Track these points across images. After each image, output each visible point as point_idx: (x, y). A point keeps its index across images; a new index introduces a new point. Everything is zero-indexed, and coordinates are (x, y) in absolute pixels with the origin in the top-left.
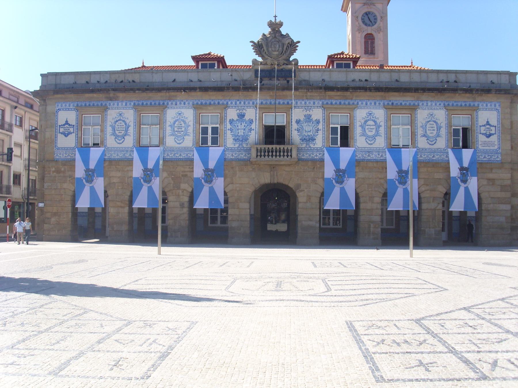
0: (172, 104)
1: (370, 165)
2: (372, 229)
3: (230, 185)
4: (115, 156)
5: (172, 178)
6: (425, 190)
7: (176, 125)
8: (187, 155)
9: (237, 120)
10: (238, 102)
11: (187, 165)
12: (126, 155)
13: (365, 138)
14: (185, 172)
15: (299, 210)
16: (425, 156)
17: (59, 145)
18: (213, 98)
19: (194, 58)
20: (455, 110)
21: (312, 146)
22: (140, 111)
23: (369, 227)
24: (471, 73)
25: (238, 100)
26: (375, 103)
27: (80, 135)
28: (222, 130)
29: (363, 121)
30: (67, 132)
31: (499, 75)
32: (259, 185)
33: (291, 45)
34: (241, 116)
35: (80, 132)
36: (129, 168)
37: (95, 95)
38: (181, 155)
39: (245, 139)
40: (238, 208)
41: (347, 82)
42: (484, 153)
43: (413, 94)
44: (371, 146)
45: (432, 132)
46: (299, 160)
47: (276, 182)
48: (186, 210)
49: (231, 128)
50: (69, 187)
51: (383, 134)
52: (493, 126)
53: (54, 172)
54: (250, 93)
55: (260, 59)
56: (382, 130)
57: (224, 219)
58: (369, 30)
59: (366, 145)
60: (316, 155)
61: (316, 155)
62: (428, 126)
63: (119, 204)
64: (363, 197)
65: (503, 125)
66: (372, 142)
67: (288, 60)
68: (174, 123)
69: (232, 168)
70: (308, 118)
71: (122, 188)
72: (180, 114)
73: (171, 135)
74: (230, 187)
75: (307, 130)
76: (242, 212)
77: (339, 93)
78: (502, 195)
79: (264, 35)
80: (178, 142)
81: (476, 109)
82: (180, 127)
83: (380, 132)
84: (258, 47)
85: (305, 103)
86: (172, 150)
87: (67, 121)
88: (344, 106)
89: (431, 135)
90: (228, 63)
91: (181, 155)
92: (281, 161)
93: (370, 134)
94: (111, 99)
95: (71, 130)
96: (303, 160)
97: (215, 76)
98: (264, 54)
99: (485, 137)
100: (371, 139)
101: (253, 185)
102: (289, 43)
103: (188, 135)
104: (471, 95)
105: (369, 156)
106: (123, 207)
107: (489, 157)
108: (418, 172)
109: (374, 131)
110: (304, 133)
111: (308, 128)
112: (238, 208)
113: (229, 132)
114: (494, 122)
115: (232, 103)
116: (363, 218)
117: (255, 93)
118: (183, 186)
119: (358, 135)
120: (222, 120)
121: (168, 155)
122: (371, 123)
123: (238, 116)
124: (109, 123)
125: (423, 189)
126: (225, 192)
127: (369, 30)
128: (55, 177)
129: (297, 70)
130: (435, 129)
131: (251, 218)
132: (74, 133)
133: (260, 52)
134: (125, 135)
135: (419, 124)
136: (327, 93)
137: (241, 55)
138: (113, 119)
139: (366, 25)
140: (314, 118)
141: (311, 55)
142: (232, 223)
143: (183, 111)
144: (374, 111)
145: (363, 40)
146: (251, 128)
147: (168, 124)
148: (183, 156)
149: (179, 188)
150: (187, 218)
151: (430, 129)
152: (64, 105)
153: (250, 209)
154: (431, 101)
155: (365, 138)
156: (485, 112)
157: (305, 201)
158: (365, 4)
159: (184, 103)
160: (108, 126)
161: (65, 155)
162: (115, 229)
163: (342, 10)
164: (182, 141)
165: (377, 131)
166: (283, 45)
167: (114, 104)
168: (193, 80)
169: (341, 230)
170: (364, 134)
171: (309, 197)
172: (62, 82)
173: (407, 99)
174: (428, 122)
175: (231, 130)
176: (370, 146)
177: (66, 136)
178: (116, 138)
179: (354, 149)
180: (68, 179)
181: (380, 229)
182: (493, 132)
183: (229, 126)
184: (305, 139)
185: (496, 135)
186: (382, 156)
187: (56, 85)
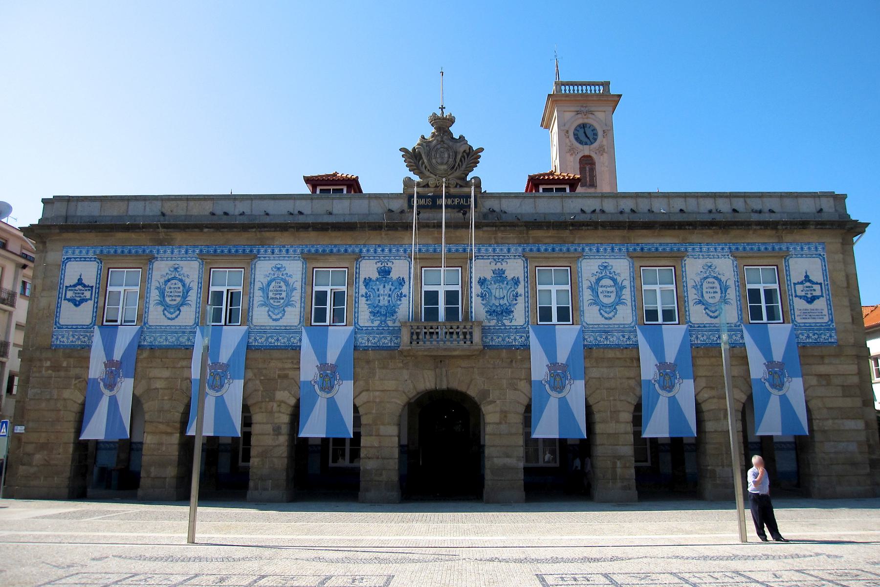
0: (266, 251)
1: (610, 354)
2: (619, 471)
3: (364, 393)
4: (161, 341)
5: (261, 381)
6: (710, 398)
7: (271, 288)
8: (289, 340)
9: (377, 279)
10: (379, 250)
11: (288, 358)
12: (181, 339)
13: (598, 307)
14: (284, 369)
15: (487, 437)
16: (705, 338)
17: (63, 321)
18: (337, 242)
19: (308, 180)
20: (750, 257)
21: (507, 322)
22: (210, 263)
23: (614, 467)
24: (771, 197)
25: (379, 246)
26: (613, 249)
27: (101, 304)
28: (351, 296)
29: (593, 279)
30: (78, 299)
31: (817, 199)
32: (415, 393)
33: (468, 155)
34: (385, 273)
35: (101, 300)
36: (184, 363)
37: (133, 235)
38: (278, 340)
39: (391, 311)
40: (378, 435)
41: (562, 214)
42: (805, 330)
43: (677, 232)
44: (610, 322)
45: (712, 295)
46: (486, 346)
47: (444, 387)
48: (283, 439)
49: (366, 294)
50: (73, 396)
51: (629, 300)
52: (817, 283)
53: (48, 368)
54: (399, 234)
55: (416, 178)
56: (627, 294)
57: (355, 454)
58: (586, 150)
59: (600, 320)
60: (515, 339)
61: (515, 339)
62: (705, 285)
63: (162, 427)
64: (599, 411)
65: (833, 282)
66: (611, 315)
67: (464, 179)
68: (269, 284)
69: (368, 362)
70: (500, 275)
71: (170, 399)
72: (279, 269)
73: (262, 305)
74: (364, 397)
75: (497, 295)
76: (383, 445)
77: (552, 233)
78: (848, 403)
79: (423, 137)
80: (274, 317)
81: (786, 256)
82: (278, 292)
83: (623, 297)
84: (413, 158)
85: (494, 250)
86: (263, 330)
87: (80, 280)
88: (561, 255)
89: (711, 301)
90: (365, 190)
91: (278, 340)
92: (455, 350)
93: (606, 301)
94: (161, 243)
95: (87, 294)
96: (490, 347)
97: (342, 207)
98: (423, 169)
99: (804, 302)
100: (608, 310)
101: (404, 392)
102: (464, 151)
103: (292, 305)
104: (774, 232)
105: (606, 338)
106: (171, 434)
107: (816, 336)
108: (693, 365)
109: (613, 295)
110: (493, 301)
111: (498, 291)
112: (378, 435)
113: (363, 301)
114: (817, 276)
115: (368, 251)
116: (602, 450)
117: (408, 233)
118: (281, 395)
119: (586, 303)
120: (352, 281)
121: (256, 340)
122: (607, 282)
123: (379, 273)
124: (154, 284)
125: (706, 396)
126: (354, 405)
127: (586, 150)
128: (50, 377)
129: (479, 195)
130: (718, 290)
131: (401, 452)
132: (91, 299)
133: (418, 168)
134: (182, 305)
135: (690, 284)
136: (530, 232)
137: (385, 176)
138: (162, 276)
139: (581, 142)
140: (510, 274)
141: (501, 174)
142: (367, 464)
143: (285, 263)
144: (611, 262)
145: (578, 166)
146: (401, 294)
147: (258, 285)
148: (283, 341)
149: (272, 399)
150: (285, 454)
151: (708, 290)
152: (77, 251)
153: (399, 436)
154: (708, 244)
155: (598, 307)
156: (800, 260)
157: (498, 421)
158: (578, 113)
159: (287, 251)
160: (153, 288)
161: (71, 338)
162: (152, 475)
163: (542, 126)
164: (281, 315)
165: (619, 295)
166: (456, 153)
167: (165, 252)
168: (305, 212)
169: (562, 478)
170: (596, 302)
171: (504, 413)
172: (79, 213)
173: (668, 240)
174: (707, 278)
175: (367, 296)
176: (607, 322)
177: (76, 305)
178: (165, 309)
179: (579, 327)
180: (74, 382)
181: (633, 471)
182: (818, 293)
183: (363, 290)
184: (494, 311)
185: (824, 299)
186: (629, 338)
187: (66, 218)
